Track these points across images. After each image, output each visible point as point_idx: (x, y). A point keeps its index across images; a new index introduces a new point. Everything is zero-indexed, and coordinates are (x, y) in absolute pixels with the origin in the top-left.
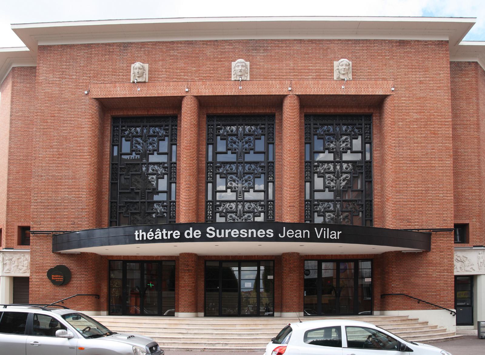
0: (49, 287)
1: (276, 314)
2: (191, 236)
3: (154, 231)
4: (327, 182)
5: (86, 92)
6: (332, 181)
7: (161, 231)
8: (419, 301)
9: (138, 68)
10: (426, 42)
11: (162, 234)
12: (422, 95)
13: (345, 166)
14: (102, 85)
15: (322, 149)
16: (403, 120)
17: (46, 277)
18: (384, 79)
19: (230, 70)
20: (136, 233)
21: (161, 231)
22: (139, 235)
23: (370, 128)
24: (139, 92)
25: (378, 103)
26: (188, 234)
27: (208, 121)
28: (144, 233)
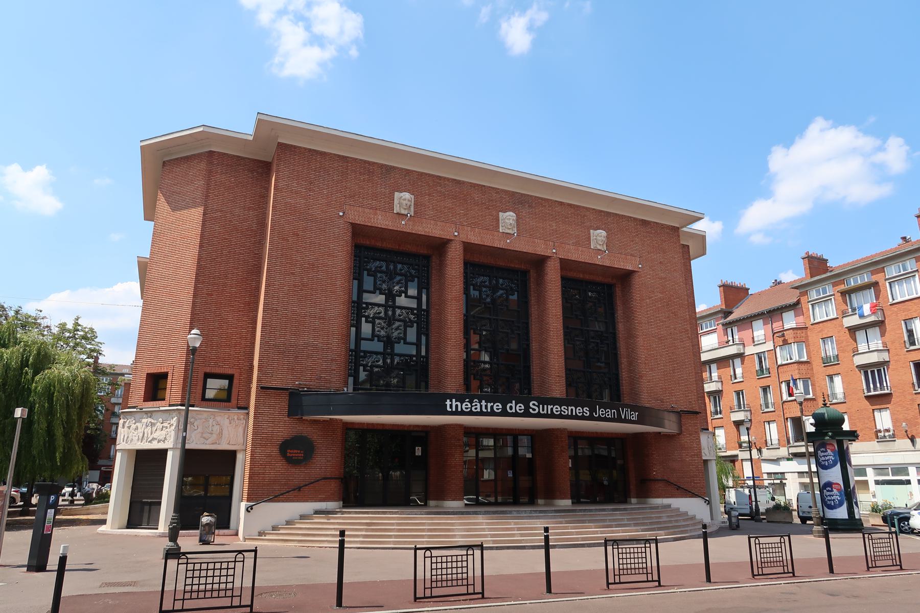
0: (280, 465)
1: (432, 503)
2: (513, 411)
3: (471, 402)
4: (377, 329)
5: (341, 214)
6: (382, 328)
7: (480, 402)
8: (679, 488)
9: (403, 200)
10: (663, 225)
11: (481, 406)
12: (663, 275)
13: (398, 312)
14: (361, 209)
15: (372, 289)
16: (650, 298)
17: (275, 451)
18: (632, 255)
19: (497, 219)
20: (448, 403)
21: (480, 402)
22: (451, 406)
23: (428, 271)
24: (403, 226)
25: (626, 277)
26: (511, 408)
27: (381, 256)
28: (459, 404)
